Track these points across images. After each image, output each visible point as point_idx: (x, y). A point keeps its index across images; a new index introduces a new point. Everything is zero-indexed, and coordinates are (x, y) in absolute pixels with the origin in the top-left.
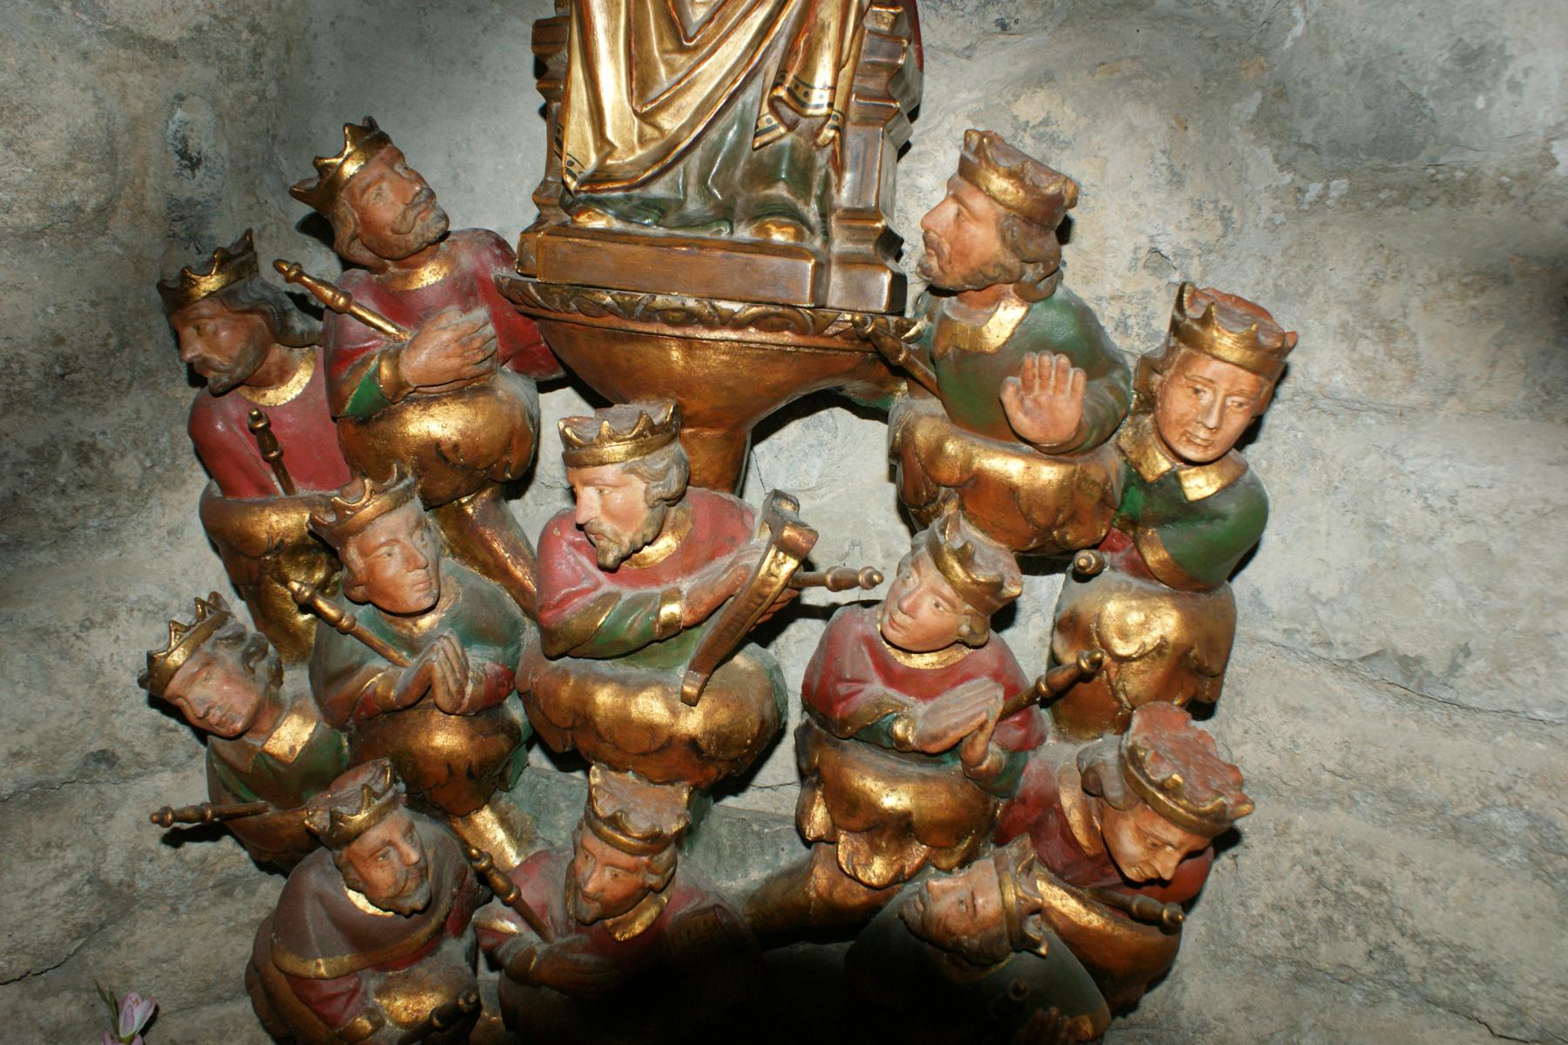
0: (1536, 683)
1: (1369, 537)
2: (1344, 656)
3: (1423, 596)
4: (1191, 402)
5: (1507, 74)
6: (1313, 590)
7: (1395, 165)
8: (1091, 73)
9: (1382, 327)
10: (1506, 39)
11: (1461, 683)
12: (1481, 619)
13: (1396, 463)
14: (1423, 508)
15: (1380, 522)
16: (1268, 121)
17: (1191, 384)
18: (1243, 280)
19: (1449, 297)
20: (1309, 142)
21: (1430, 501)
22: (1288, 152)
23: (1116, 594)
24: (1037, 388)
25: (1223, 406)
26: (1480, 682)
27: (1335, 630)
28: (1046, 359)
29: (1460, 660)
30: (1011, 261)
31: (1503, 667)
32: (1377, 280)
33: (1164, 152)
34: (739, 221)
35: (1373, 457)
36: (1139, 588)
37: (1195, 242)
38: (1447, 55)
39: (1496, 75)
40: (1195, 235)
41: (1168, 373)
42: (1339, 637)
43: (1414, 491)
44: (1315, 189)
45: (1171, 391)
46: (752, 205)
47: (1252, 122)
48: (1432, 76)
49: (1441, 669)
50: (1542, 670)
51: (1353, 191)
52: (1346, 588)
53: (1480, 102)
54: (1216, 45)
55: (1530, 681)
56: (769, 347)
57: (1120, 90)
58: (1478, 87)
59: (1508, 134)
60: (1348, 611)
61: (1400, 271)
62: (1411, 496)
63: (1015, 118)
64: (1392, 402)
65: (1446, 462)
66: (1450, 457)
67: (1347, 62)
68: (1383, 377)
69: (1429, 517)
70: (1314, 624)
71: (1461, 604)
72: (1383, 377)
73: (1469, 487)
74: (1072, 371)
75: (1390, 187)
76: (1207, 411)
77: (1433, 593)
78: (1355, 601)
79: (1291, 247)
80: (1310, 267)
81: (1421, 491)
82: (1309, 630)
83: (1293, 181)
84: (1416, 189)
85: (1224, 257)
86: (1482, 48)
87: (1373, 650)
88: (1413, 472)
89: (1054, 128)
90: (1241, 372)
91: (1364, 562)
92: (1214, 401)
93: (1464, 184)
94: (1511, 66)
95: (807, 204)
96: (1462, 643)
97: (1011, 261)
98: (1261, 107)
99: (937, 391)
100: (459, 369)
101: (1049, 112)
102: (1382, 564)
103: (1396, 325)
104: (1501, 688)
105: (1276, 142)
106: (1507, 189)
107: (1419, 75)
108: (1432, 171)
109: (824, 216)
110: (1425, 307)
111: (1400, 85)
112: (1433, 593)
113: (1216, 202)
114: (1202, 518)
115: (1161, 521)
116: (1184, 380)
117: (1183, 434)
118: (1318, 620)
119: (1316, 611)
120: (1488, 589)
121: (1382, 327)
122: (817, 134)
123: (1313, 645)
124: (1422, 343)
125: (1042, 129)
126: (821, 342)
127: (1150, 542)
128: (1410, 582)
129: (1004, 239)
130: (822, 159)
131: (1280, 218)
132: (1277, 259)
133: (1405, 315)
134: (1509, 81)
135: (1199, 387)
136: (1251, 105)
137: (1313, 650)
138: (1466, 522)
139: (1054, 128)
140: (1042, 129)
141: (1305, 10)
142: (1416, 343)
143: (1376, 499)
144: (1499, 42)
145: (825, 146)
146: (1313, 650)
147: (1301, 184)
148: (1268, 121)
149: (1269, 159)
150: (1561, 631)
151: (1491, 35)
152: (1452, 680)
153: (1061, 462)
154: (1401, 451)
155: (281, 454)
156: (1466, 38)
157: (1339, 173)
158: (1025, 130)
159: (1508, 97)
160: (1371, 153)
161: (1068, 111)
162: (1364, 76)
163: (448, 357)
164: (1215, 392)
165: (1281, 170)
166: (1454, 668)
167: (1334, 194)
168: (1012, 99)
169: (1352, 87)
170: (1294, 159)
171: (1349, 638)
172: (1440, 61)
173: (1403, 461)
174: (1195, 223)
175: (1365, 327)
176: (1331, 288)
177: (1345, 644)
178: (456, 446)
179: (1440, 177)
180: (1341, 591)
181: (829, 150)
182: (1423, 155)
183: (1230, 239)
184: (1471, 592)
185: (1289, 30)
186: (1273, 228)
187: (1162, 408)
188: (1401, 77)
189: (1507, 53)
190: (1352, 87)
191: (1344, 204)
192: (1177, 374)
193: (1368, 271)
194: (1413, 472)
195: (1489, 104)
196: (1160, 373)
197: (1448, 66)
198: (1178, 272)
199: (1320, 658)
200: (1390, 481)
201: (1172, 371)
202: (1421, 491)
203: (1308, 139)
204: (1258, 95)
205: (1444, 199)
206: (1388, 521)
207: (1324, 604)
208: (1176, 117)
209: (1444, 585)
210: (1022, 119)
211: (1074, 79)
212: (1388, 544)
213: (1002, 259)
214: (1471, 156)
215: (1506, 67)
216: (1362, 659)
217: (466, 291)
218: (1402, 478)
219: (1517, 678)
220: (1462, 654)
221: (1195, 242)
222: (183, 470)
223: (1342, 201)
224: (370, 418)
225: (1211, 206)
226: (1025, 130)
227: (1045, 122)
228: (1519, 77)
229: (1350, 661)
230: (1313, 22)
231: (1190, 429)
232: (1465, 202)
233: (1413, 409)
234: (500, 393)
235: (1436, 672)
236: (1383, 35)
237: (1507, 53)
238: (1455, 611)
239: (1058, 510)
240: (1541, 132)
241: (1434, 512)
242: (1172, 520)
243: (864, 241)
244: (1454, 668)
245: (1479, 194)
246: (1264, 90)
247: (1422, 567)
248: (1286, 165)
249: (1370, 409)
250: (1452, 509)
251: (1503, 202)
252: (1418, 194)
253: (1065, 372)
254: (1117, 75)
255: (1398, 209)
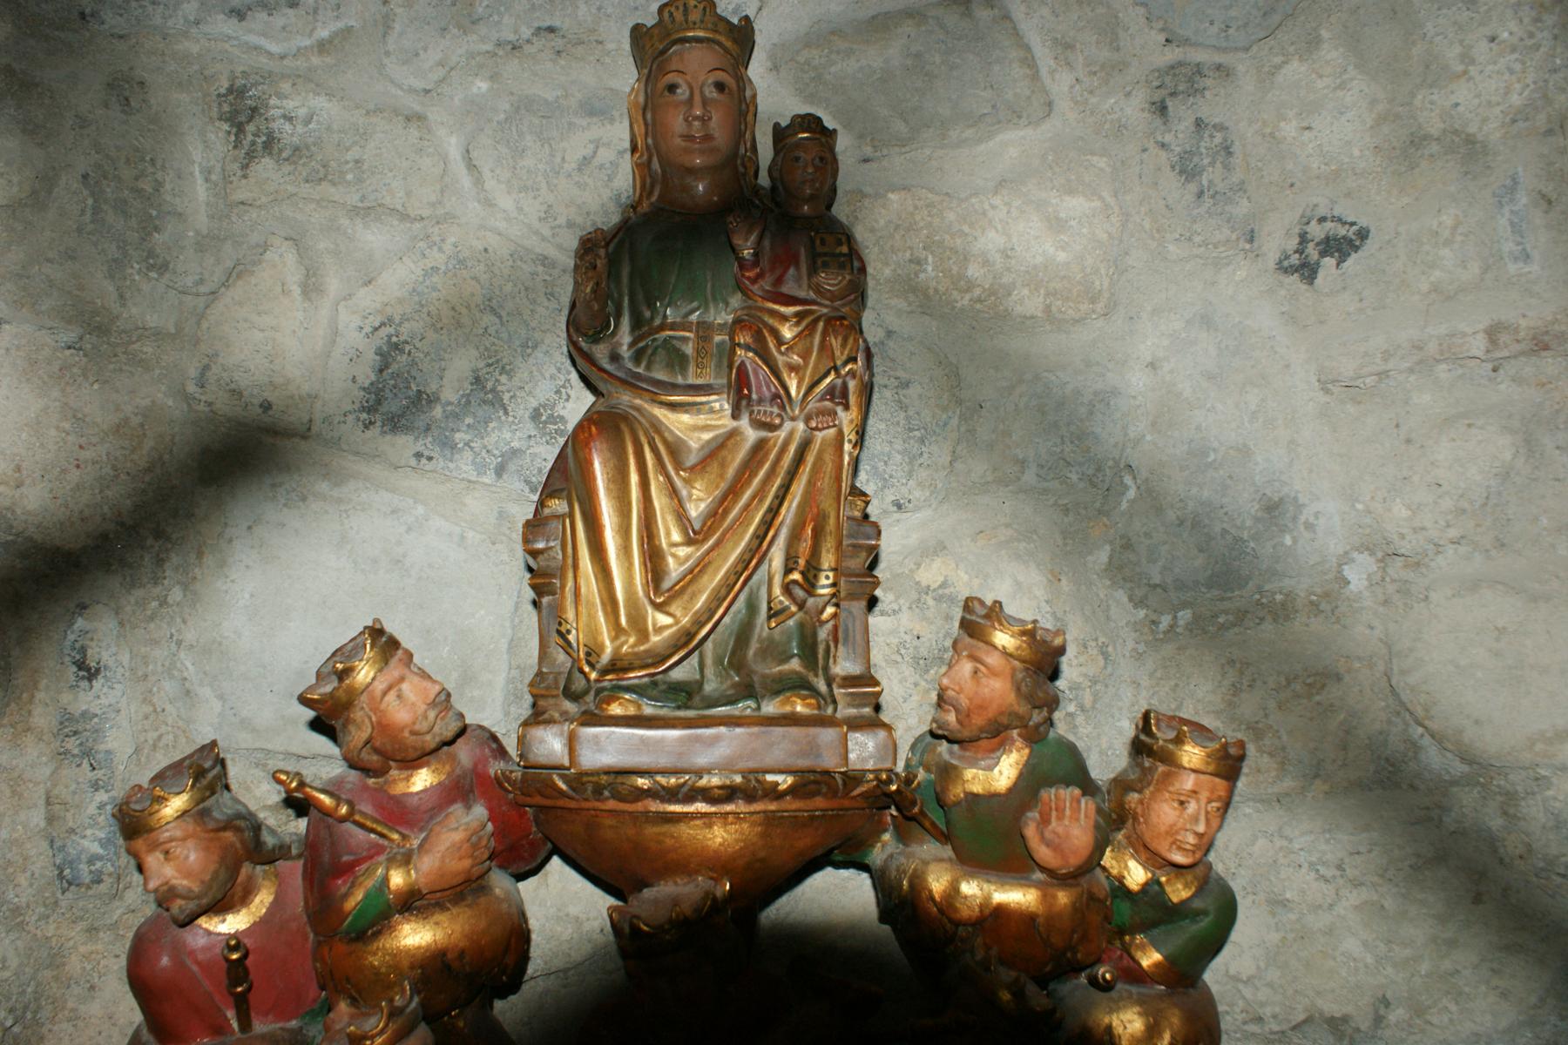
0: (1451, 1020)
1: (1274, 914)
2: (1276, 1028)
3: (1334, 959)
4: (1177, 813)
5: (1302, 518)
6: (1232, 972)
7: (1230, 595)
8: (974, 540)
9: (1248, 728)
10: (1297, 492)
11: (1387, 1033)
12: (1390, 970)
13: (1285, 843)
14: (1316, 879)
15: (1280, 898)
16: (1120, 568)
17: (1175, 797)
18: (1120, 704)
19: (1298, 696)
20: (1158, 582)
21: (1321, 872)
22: (1139, 593)
23: (1121, 1004)
24: (1053, 819)
25: (1207, 813)
26: (1403, 1029)
27: (1262, 1005)
28: (1062, 791)
29: (1382, 1012)
30: (1022, 709)
31: (1419, 1011)
32: (1236, 690)
33: (1047, 602)
34: (763, 697)
35: (1261, 842)
36: (1139, 993)
37: (1085, 675)
38: (1257, 507)
39: (1295, 519)
40: (1083, 669)
41: (1147, 792)
42: (1267, 1012)
43: (1306, 865)
44: (1166, 621)
45: (1155, 806)
46: (768, 681)
47: (1106, 570)
48: (1248, 523)
49: (1367, 1024)
50: (1453, 1008)
51: (1197, 618)
52: (1262, 965)
53: (1288, 541)
54: (1067, 510)
55: (1446, 1019)
56: (800, 814)
57: (1003, 552)
58: (1283, 530)
59: (1311, 563)
60: (1270, 985)
61: (1254, 680)
62: (1304, 870)
63: (918, 583)
64: (1270, 791)
65: (1328, 836)
66: (1329, 831)
67: (1178, 518)
68: (1259, 771)
69: (1324, 886)
70: (1241, 1003)
71: (1369, 959)
72: (1259, 771)
73: (1352, 854)
74: (1083, 801)
75: (1226, 612)
76: (1195, 819)
77: (1343, 954)
78: (1273, 975)
79: (1155, 671)
80: (1177, 685)
81: (1311, 864)
82: (1238, 1010)
83: (1147, 616)
84: (1247, 612)
85: (1106, 686)
86: (1281, 499)
87: (1301, 1017)
88: (1302, 849)
89: (952, 589)
90: (1217, 780)
91: (1275, 937)
92: (1199, 808)
93: (1283, 604)
94: (1305, 512)
95: (816, 675)
96: (1380, 996)
97: (1022, 709)
98: (1111, 558)
99: (944, 837)
100: (469, 871)
101: (946, 576)
102: (1291, 936)
103: (1260, 725)
104: (1422, 1031)
105: (1128, 585)
106: (1317, 606)
107: (1238, 523)
108: (1257, 596)
109: (829, 685)
110: (1280, 708)
111: (1225, 532)
112: (1343, 954)
113: (1096, 640)
114: (1186, 917)
115: (1145, 927)
116: (1167, 795)
117: (1173, 843)
118: (1244, 998)
119: (1239, 991)
120: (1390, 942)
121: (1248, 728)
122: (822, 612)
123: (1245, 1023)
124: (1285, 738)
125: (940, 592)
126: (846, 803)
127: (1142, 947)
128: (1320, 948)
129: (1018, 689)
130: (823, 634)
131: (1141, 648)
132: (1145, 682)
133: (1266, 716)
134: (1305, 523)
135: (1182, 798)
136: (1103, 555)
137: (1246, 1027)
138: (1356, 886)
139: (952, 589)
140: (940, 592)
141: (1135, 478)
142: (1279, 738)
143: (1273, 879)
144: (1293, 494)
145: (827, 621)
146: (1246, 1027)
147: (1154, 617)
148: (1120, 568)
149: (1125, 599)
150: (1459, 968)
151: (1286, 490)
152: (1380, 1032)
153: (1071, 886)
154: (1288, 831)
155: (249, 989)
156: (1268, 492)
157: (1185, 605)
158: (927, 594)
159: (1307, 535)
160: (1210, 587)
161: (962, 574)
162: (1193, 527)
163: (460, 859)
164: (1198, 801)
165: (1136, 606)
166: (1378, 1020)
167: (1181, 623)
168: (914, 567)
169: (1185, 535)
170: (1146, 597)
171: (1277, 1010)
172: (1253, 511)
173: (1291, 841)
174: (1082, 659)
175: (1234, 730)
176: (1198, 701)
177: (1275, 1017)
178: (462, 953)
179: (1264, 600)
180: (1258, 968)
181: (830, 625)
182: (1251, 584)
183: (1109, 669)
184: (1376, 947)
185: (1124, 494)
186: (1138, 656)
187: (1146, 822)
188: (1225, 525)
189: (1301, 502)
190: (1185, 535)
191: (1191, 631)
192: (1158, 790)
193: (1225, 682)
194: (1302, 849)
195: (1295, 540)
196: (1140, 791)
197: (1259, 514)
198: (1073, 704)
199: (1253, 1034)
200: (1282, 860)
201: (1151, 788)
202: (1311, 864)
203: (1157, 580)
204: (1108, 547)
205: (1269, 618)
206: (1288, 896)
207: (1245, 983)
208: (1052, 572)
209: (1351, 945)
210: (924, 583)
211: (961, 547)
212: (1293, 917)
213: (1016, 708)
214: (1287, 582)
215: (1301, 512)
216: (1294, 1028)
217: (455, 791)
218: (1292, 856)
219: (1435, 1020)
220: (1382, 1006)
221: (1085, 675)
222: (43, 1024)
223: (1189, 628)
224: (365, 932)
225: (1094, 644)
226: (927, 594)
227: (944, 585)
228: (1312, 519)
229: (1283, 1032)
230: (1143, 488)
231: (1179, 838)
232: (1287, 618)
233: (1287, 794)
234: (497, 891)
235: (1363, 1028)
236: (1206, 494)
237: (1301, 502)
238: (1366, 966)
239: (1073, 931)
240: (1334, 560)
241: (1327, 881)
242: (1154, 924)
243: (865, 705)
244: (1378, 1020)
245: (1297, 611)
246: (1111, 543)
247: (1329, 931)
248: (1139, 603)
249: (1248, 800)
250: (1342, 876)
251: (1316, 616)
252: (1249, 616)
253: (1079, 802)
254: (993, 541)
255: (1236, 630)
